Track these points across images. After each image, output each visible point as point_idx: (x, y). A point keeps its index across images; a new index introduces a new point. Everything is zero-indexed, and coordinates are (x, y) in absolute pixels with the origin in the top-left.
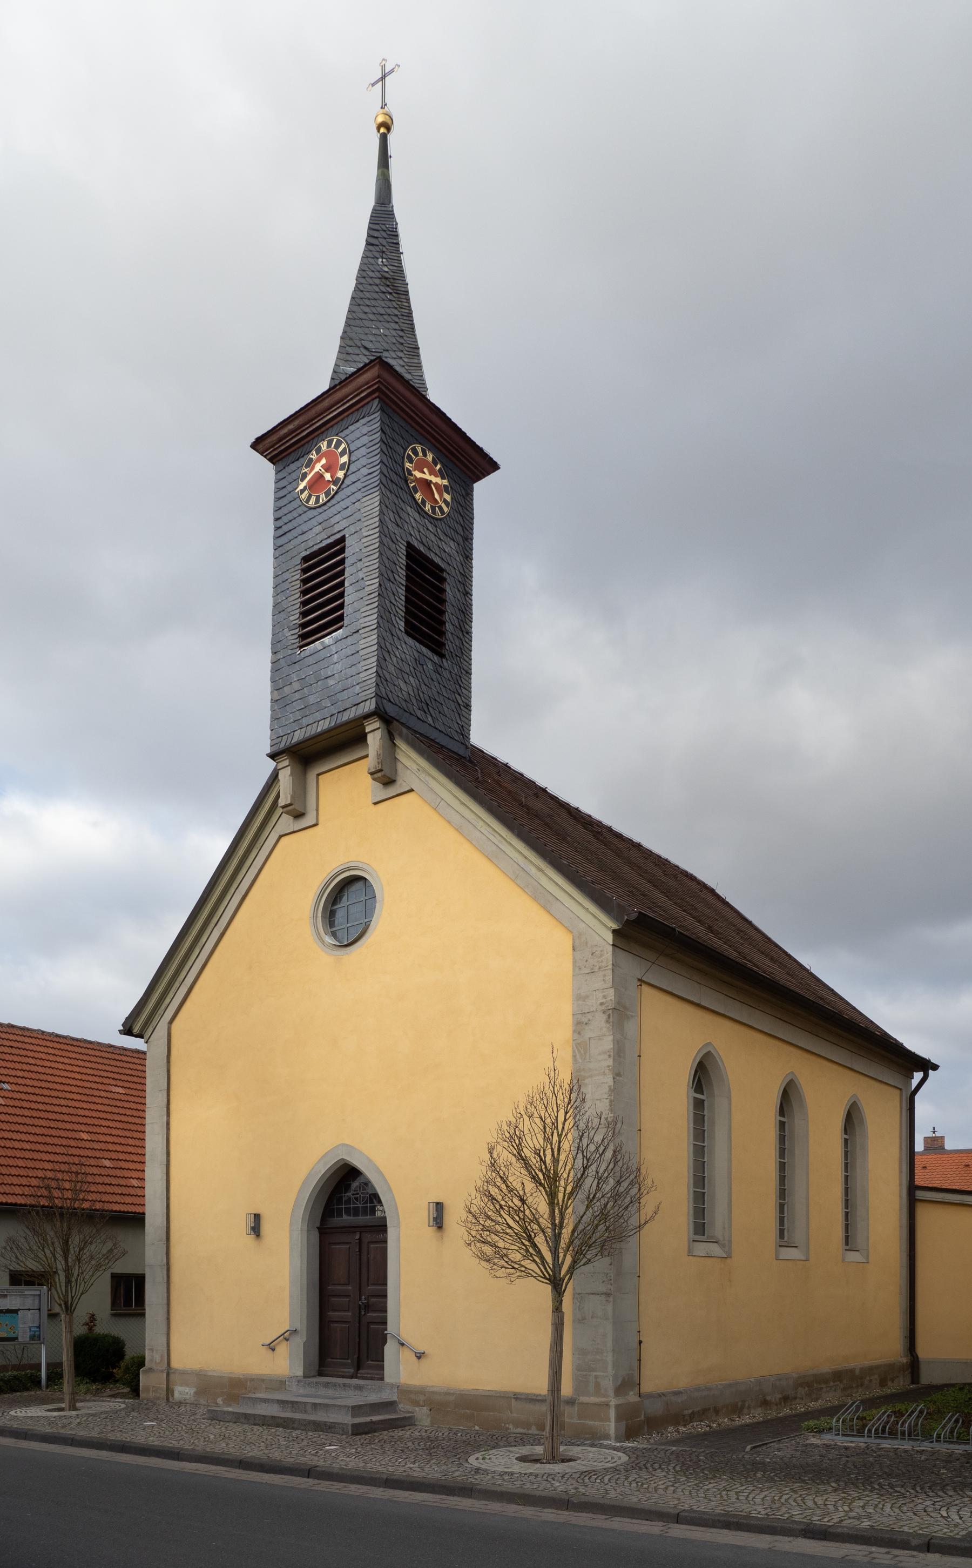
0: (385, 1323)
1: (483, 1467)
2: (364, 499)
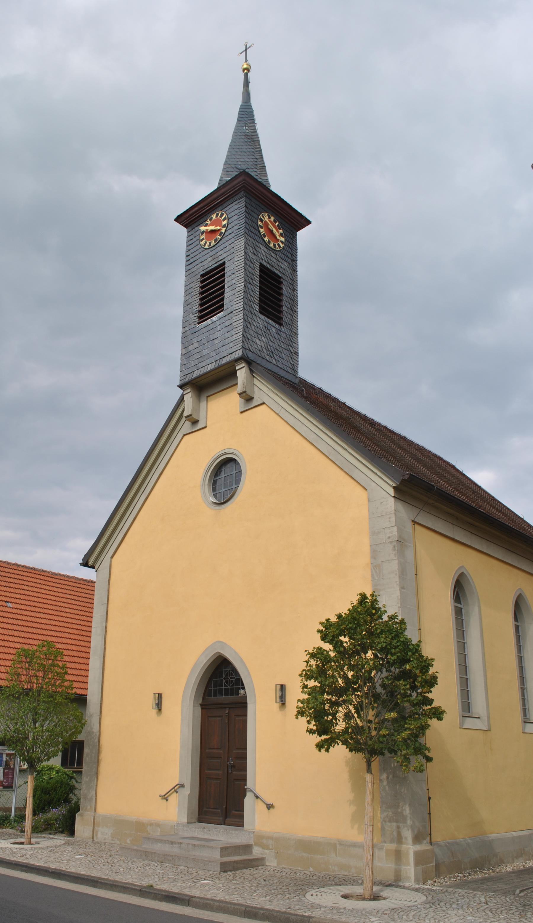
0: (245, 780)
1: (317, 902)
2: (236, 242)
